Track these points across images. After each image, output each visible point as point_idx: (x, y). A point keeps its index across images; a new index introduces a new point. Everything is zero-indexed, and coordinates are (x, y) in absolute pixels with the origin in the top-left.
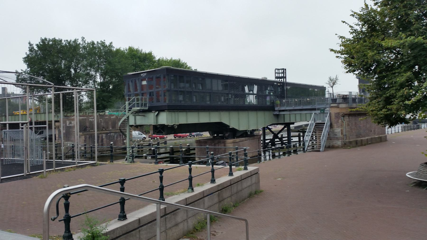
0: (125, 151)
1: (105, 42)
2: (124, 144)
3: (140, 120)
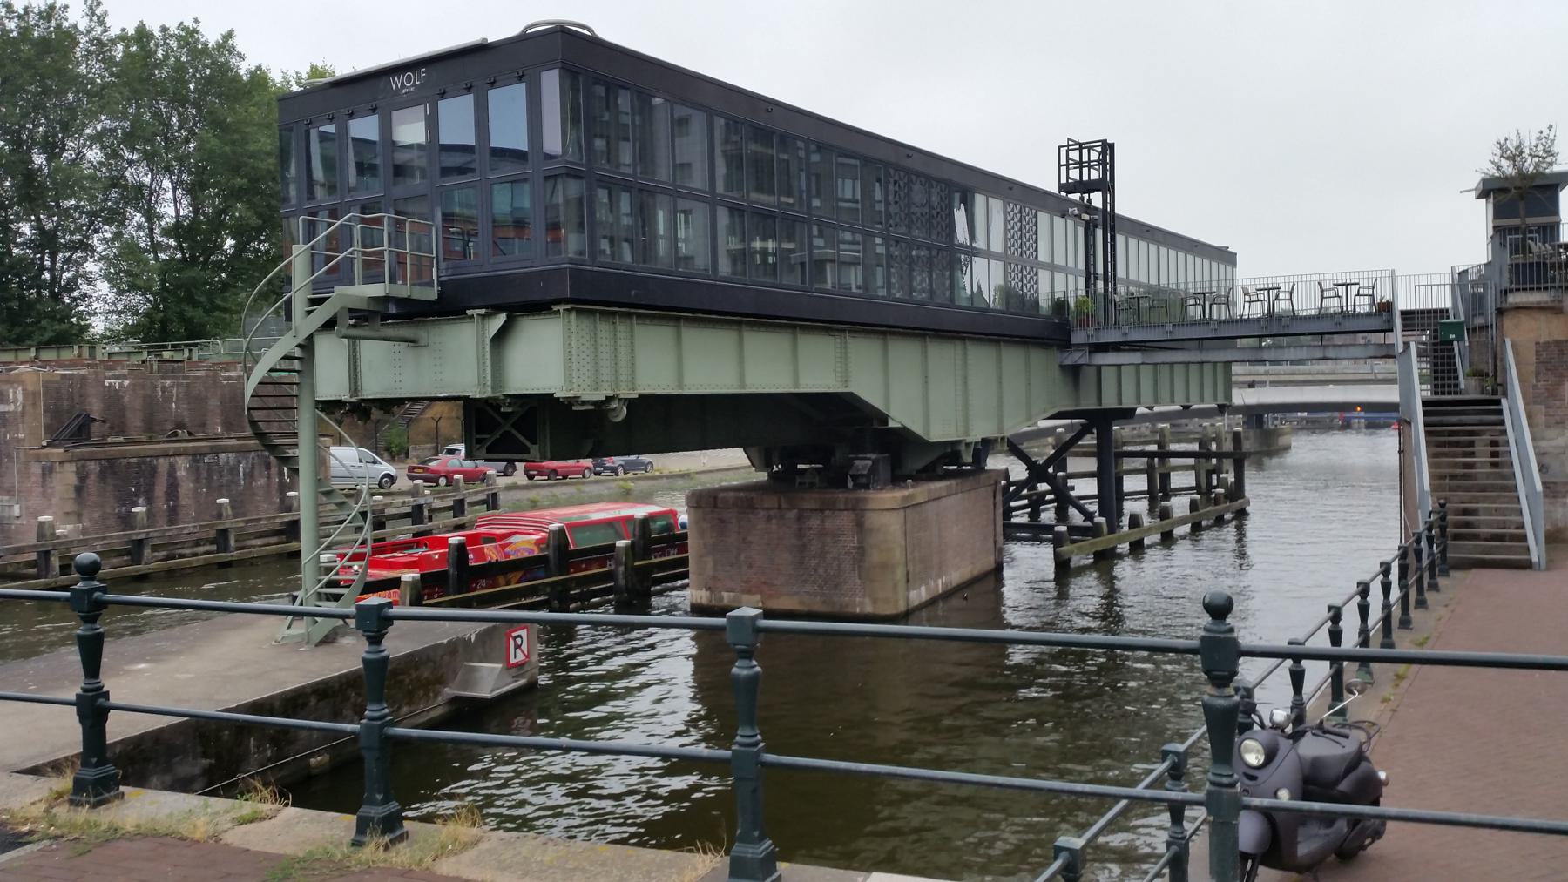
0: (293, 546)
1: (201, 27)
2: (289, 509)
3: (385, 369)
